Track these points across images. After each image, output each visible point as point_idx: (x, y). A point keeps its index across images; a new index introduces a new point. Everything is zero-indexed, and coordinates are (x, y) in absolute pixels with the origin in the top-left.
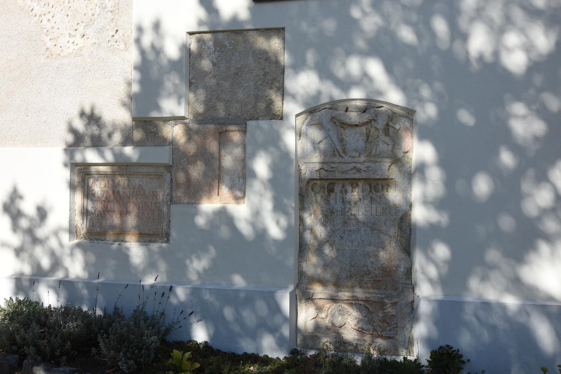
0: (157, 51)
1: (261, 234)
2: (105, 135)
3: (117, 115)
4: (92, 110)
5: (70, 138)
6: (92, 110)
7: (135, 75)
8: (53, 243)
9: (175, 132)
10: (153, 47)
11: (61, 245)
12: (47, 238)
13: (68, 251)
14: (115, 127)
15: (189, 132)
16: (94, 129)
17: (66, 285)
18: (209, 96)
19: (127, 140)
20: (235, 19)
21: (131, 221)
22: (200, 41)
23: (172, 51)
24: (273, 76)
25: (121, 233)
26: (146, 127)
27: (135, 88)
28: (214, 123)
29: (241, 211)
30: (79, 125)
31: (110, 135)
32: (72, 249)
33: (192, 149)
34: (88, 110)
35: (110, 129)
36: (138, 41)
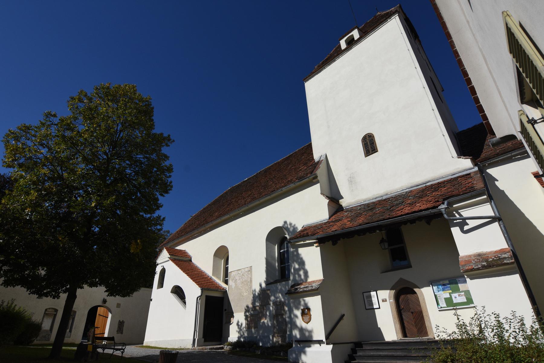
0: (255, 294)
1: (268, 325)
3: (251, 306)
17: (244, 338)
23: (257, 294)
24: (269, 297)
26: (254, 307)
28: (262, 306)
29: (266, 321)
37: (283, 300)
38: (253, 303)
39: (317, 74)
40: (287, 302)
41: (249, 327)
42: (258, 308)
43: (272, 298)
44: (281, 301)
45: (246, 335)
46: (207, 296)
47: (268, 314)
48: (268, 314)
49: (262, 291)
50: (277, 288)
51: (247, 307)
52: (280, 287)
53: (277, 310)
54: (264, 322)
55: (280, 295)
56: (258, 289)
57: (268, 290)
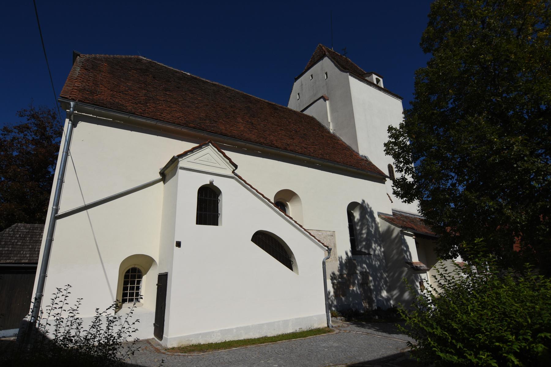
3: (337, 273)
17: (335, 306)
19: (339, 278)
23: (344, 262)
24: (355, 268)
26: (341, 275)
29: (355, 289)
37: (368, 270)
38: (341, 270)
39: (359, 80)
43: (359, 268)
45: (335, 303)
47: (356, 282)
48: (356, 282)
49: (349, 259)
51: (333, 274)
53: (363, 279)
54: (353, 290)
56: (344, 257)
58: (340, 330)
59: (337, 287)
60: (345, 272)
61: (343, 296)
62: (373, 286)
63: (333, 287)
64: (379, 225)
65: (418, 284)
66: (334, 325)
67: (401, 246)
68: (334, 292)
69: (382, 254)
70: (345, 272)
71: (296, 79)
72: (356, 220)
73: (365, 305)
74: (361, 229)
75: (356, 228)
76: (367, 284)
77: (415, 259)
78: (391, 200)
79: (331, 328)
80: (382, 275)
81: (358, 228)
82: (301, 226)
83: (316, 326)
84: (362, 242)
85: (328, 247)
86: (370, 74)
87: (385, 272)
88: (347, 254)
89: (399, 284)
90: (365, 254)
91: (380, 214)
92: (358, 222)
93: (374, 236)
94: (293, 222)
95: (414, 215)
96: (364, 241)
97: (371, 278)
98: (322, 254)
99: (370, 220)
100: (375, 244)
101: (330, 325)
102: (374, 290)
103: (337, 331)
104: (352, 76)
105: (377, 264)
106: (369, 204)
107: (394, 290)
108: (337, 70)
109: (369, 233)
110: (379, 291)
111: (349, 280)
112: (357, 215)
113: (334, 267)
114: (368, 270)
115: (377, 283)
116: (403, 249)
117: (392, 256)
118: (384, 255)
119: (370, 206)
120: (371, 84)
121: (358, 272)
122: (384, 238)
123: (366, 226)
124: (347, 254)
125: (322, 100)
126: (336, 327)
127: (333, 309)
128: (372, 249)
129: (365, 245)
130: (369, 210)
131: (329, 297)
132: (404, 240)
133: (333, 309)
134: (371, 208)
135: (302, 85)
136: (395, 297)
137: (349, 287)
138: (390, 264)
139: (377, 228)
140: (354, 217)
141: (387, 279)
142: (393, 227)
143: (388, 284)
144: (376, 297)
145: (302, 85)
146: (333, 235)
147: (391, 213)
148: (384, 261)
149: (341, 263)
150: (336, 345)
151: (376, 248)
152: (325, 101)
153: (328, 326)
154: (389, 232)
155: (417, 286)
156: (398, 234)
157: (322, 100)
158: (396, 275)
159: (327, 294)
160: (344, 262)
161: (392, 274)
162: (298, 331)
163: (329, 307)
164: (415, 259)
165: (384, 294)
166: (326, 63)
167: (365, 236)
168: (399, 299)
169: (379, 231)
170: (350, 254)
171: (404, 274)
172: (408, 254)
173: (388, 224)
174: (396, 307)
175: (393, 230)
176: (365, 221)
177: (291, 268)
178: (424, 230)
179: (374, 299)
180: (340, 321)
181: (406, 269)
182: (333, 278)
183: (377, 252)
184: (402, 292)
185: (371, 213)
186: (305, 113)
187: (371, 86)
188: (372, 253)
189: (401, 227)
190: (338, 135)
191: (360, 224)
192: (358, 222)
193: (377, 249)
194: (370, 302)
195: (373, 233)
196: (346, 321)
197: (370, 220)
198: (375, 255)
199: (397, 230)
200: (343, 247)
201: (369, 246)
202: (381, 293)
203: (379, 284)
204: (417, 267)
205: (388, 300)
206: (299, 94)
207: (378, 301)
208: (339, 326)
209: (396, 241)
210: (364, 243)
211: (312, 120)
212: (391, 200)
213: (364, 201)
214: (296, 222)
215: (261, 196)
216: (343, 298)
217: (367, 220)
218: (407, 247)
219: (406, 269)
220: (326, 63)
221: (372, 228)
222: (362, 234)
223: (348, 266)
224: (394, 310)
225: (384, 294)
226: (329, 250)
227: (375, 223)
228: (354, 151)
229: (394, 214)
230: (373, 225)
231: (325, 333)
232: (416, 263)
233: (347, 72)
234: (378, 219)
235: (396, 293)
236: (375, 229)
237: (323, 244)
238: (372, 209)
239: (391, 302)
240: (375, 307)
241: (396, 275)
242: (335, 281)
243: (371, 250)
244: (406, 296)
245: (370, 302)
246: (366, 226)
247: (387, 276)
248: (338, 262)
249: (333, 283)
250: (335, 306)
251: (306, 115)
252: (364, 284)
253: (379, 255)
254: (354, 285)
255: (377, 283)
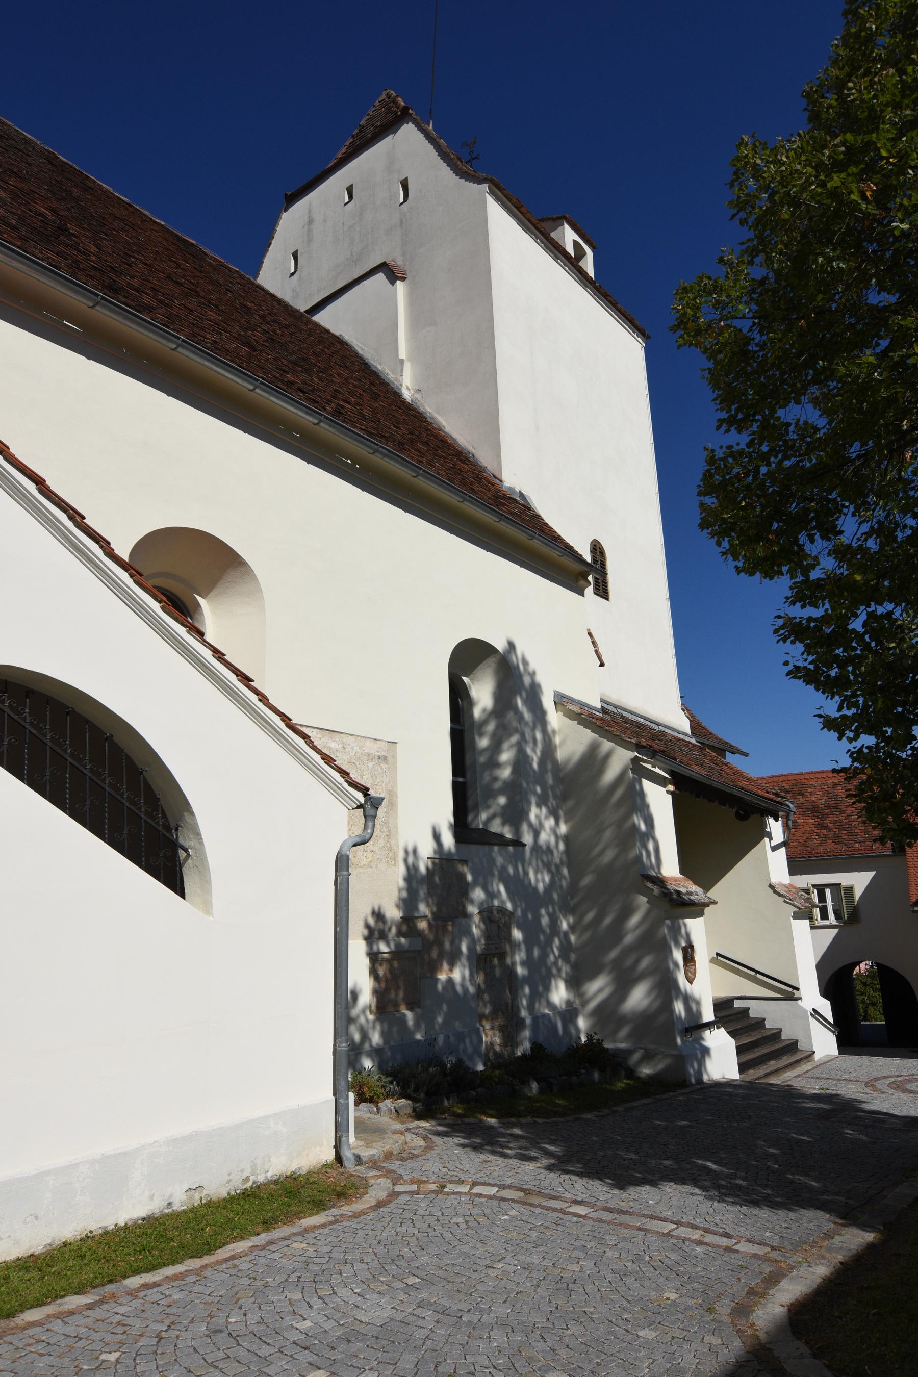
0: (416, 868)
1: (466, 991)
2: (386, 929)
3: (393, 913)
4: (379, 909)
5: (366, 932)
6: (379, 909)
7: (402, 883)
8: (362, 1020)
9: (422, 925)
10: (413, 865)
11: (367, 1021)
12: (358, 1016)
13: (371, 1025)
14: (393, 921)
15: (429, 924)
16: (381, 925)
17: (377, 1053)
18: (430, 900)
19: (400, 934)
20: (450, 850)
21: (401, 994)
22: (433, 863)
23: (423, 869)
24: (464, 891)
25: (396, 1005)
26: (409, 920)
27: (405, 894)
28: (440, 920)
29: (457, 975)
30: (371, 921)
31: (390, 929)
32: (374, 1022)
33: (431, 937)
34: (376, 909)
35: (389, 924)
36: (406, 861)
37: (509, 906)
38: (408, 903)
39: (521, 223)
40: (519, 912)
41: (384, 1005)
42: (422, 925)
43: (478, 894)
44: (502, 910)
45: (376, 1038)
46: (707, 888)
47: (464, 948)
48: (464, 948)
49: (442, 860)
50: (493, 862)
51: (378, 915)
52: (500, 861)
53: (488, 935)
54: (450, 981)
55: (502, 889)
56: (427, 849)
57: (464, 862)
58: (397, 1179)
59: (391, 970)
60: (423, 908)
61: (410, 1009)
62: (523, 964)
63: (373, 972)
64: (557, 740)
65: (678, 955)
66: (366, 1153)
67: (628, 815)
68: (375, 992)
69: (562, 846)
70: (423, 908)
71: (291, 199)
72: (477, 713)
73: (491, 1036)
74: (496, 747)
75: (473, 743)
76: (502, 956)
77: (670, 867)
78: (599, 658)
79: (349, 1164)
80: (554, 923)
81: (484, 743)
82: (246, 680)
83: (279, 1162)
84: (490, 794)
85: (365, 791)
86: (557, 221)
87: (568, 909)
88: (437, 837)
89: (613, 954)
90: (500, 840)
91: (561, 701)
92: (484, 722)
93: (539, 778)
94: (207, 654)
95: (658, 724)
96: (501, 791)
97: (517, 934)
98: (337, 821)
99: (527, 716)
100: (539, 806)
101: (347, 1154)
102: (526, 980)
103: (379, 1188)
104: (497, 199)
105: (539, 879)
106: (529, 658)
107: (592, 976)
108: (445, 172)
109: (521, 762)
110: (541, 980)
111: (439, 943)
112: (482, 693)
113: (381, 889)
114: (509, 906)
115: (536, 952)
116: (635, 828)
117: (598, 849)
118: (567, 851)
119: (531, 669)
120: (555, 249)
121: (473, 909)
122: (571, 786)
123: (515, 739)
124: (437, 837)
125: (381, 277)
126: (374, 1164)
127: (367, 1063)
128: (530, 825)
129: (505, 808)
130: (527, 680)
131: (354, 1012)
132: (642, 794)
133: (367, 1063)
134: (533, 675)
135: (311, 221)
136: (592, 1005)
137: (434, 968)
138: (587, 880)
139: (549, 749)
140: (471, 703)
141: (573, 938)
142: (607, 745)
143: (573, 957)
144: (531, 1008)
145: (311, 221)
146: (386, 757)
147: (598, 705)
148: (565, 871)
149: (411, 875)
150: (376, 1311)
151: (541, 825)
152: (393, 283)
153: (339, 1159)
154: (592, 762)
155: (676, 965)
156: (623, 774)
157: (381, 277)
158: (607, 921)
159: (344, 998)
160: (423, 869)
161: (590, 916)
162: (180, 1200)
163: (347, 1056)
164: (670, 867)
165: (559, 994)
166: (408, 148)
167: (506, 773)
168: (606, 1015)
169: (555, 762)
170: (448, 840)
171: (634, 920)
172: (651, 846)
173: (588, 736)
174: (600, 1043)
175: (608, 755)
176: (510, 715)
177: (176, 884)
178: (696, 768)
179: (524, 1013)
180: (394, 1128)
181: (642, 900)
182: (373, 935)
183: (544, 837)
184: (623, 986)
185: (533, 694)
186: (317, 318)
187: (556, 258)
188: (528, 839)
189: (638, 747)
190: (429, 408)
191: (491, 727)
192: (484, 722)
193: (546, 827)
194: (511, 1027)
195: (535, 765)
196: (419, 1116)
197: (527, 716)
198: (536, 847)
199: (620, 758)
200: (423, 813)
201: (515, 815)
202: (547, 989)
203: (544, 955)
204: (678, 893)
205: (570, 1014)
206: (295, 255)
207: (537, 1019)
208: (388, 1156)
209: (619, 792)
210: (502, 800)
211: (337, 348)
212: (599, 658)
213: (511, 646)
214: (219, 655)
215: (31, 487)
216: (409, 1015)
217: (520, 717)
218: (649, 821)
219: (642, 900)
220: (408, 148)
221: (534, 751)
222: (498, 765)
223: (438, 885)
224: (593, 1054)
225: (559, 994)
226: (370, 805)
227: (544, 731)
228: (483, 470)
229: (604, 710)
230: (539, 736)
231: (319, 1205)
232: (676, 879)
233: (480, 182)
234: (555, 719)
235: (598, 987)
236: (543, 753)
237: (344, 773)
238: (539, 678)
239: (582, 1023)
240: (524, 1047)
241: (607, 921)
242: (383, 947)
243: (525, 827)
244: (638, 997)
245: (511, 1027)
246: (515, 739)
247: (572, 928)
248: (401, 870)
249: (374, 957)
250: (377, 1053)
251: (317, 325)
252: (490, 959)
253: (549, 850)
254: (453, 958)
255: (536, 952)
